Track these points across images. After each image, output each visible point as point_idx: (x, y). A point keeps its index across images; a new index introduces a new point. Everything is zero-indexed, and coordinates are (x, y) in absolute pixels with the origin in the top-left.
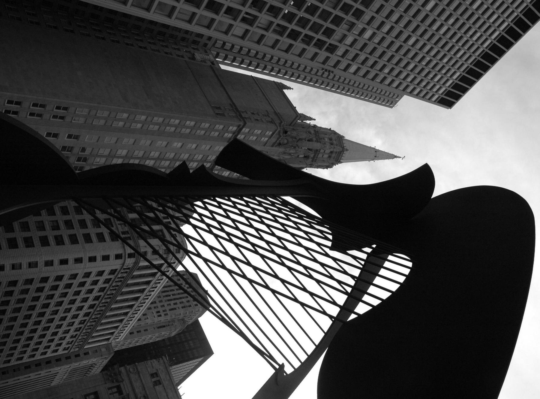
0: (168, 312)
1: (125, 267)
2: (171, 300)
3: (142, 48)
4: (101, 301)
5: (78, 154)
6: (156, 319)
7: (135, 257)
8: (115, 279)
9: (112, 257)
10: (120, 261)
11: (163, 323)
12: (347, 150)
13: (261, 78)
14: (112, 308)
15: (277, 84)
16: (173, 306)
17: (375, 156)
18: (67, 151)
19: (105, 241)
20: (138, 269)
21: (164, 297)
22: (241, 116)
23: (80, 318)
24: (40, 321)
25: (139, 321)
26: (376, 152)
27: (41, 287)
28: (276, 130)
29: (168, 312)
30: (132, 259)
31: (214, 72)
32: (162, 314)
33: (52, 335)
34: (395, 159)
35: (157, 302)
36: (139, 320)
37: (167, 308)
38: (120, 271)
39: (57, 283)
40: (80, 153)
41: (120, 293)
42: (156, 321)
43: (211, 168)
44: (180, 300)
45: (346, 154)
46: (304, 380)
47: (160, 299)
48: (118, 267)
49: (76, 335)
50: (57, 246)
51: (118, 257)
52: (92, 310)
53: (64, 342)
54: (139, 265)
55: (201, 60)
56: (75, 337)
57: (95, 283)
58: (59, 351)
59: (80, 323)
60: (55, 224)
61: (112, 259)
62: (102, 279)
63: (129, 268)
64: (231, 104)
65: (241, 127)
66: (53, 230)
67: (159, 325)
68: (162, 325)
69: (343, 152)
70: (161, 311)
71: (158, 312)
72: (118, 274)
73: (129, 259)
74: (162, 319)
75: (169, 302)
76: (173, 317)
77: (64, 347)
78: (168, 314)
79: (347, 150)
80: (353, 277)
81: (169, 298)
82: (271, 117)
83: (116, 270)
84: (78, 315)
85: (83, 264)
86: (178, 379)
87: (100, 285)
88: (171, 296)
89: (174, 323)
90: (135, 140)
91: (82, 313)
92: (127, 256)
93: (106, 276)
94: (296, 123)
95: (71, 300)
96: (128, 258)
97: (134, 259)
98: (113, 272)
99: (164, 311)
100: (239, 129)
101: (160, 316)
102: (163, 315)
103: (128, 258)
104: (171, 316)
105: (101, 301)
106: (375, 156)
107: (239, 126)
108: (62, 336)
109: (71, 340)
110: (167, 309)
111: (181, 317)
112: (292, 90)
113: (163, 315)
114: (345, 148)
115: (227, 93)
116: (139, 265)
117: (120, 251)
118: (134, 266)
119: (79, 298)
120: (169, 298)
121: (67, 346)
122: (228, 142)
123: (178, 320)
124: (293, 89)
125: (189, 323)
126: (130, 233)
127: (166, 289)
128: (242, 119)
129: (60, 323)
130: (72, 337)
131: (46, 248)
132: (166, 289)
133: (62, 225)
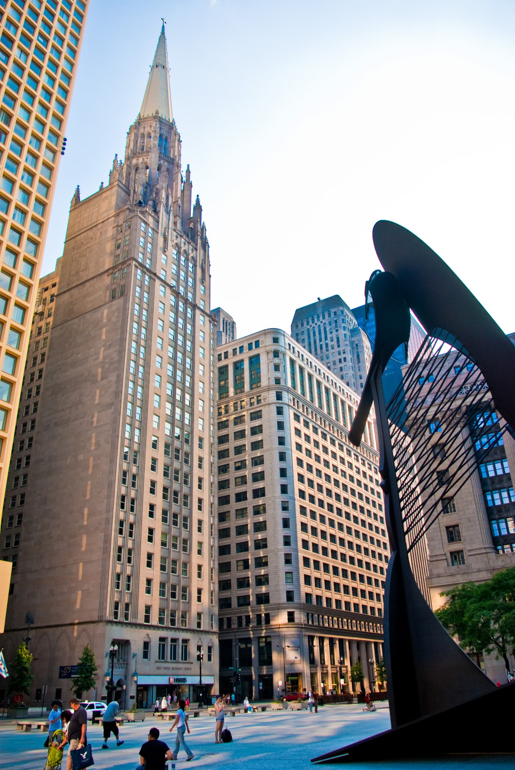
0: (341, 349)
1: (292, 403)
2: (327, 345)
3: (33, 378)
4: (311, 420)
5: (171, 458)
6: (349, 364)
7: (281, 392)
8: (313, 422)
9: (280, 418)
10: (285, 409)
11: (353, 356)
12: (157, 113)
13: (67, 230)
14: (344, 425)
15: (73, 208)
16: (335, 342)
17: (163, 68)
18: (168, 471)
19: (261, 426)
20: (304, 395)
21: (322, 352)
22: (123, 263)
23: (336, 449)
24: (318, 485)
25: (350, 384)
26: (157, 66)
27: (309, 497)
28: (140, 218)
29: (341, 349)
30: (283, 395)
31: (65, 292)
32: (342, 356)
33: (353, 481)
34: (166, 35)
35: (327, 361)
36: (348, 384)
37: (336, 349)
38: (295, 409)
39: (306, 480)
40: (170, 456)
41: (302, 396)
42: (351, 364)
43: (175, 295)
44: (328, 333)
45: (162, 114)
46: (466, 285)
47: (325, 357)
48: (292, 412)
49: (355, 454)
50: (265, 480)
51: (280, 411)
52: (319, 431)
53: (362, 468)
54: (290, 387)
55: (43, 304)
56: (370, 465)
57: (307, 438)
58: (377, 478)
59: (350, 455)
60: (240, 480)
61: (282, 418)
62: (304, 430)
63: (294, 399)
64: (107, 274)
65: (137, 264)
66: (246, 483)
67: (356, 361)
68: (356, 358)
69: (160, 118)
70: (339, 357)
71: (340, 361)
72: (299, 412)
73: (283, 399)
74: (349, 357)
75: (330, 348)
76: (348, 343)
77: (353, 459)
78: (343, 348)
79: (157, 113)
80: (506, 522)
81: (324, 347)
82: (122, 222)
83: (295, 414)
84: (332, 452)
85: (286, 452)
86: (417, 334)
87: (310, 432)
88: (321, 343)
89: (356, 343)
90: (155, 394)
91: (331, 448)
92: (280, 401)
93: (301, 426)
94: (124, 186)
95: (325, 465)
96: (282, 400)
97: (283, 393)
98: (297, 418)
99: (339, 354)
100: (139, 267)
101: (345, 359)
102: (344, 356)
103: (282, 400)
104: (347, 345)
105: (311, 420)
106: (163, 68)
107: (136, 267)
108: (355, 472)
109: (367, 465)
110: (338, 349)
111: (348, 334)
112: (79, 188)
113: (344, 356)
114: (154, 115)
115: (93, 278)
116: (290, 387)
117: (274, 409)
118: (292, 394)
119: (332, 461)
120: (324, 347)
121: (360, 461)
122: (155, 280)
123: (352, 336)
124: (78, 186)
125: (356, 323)
126: (252, 396)
127: (313, 350)
128: (128, 263)
129: (304, 451)
130: (364, 464)
131: (267, 492)
132: (313, 350)
133: (242, 539)
